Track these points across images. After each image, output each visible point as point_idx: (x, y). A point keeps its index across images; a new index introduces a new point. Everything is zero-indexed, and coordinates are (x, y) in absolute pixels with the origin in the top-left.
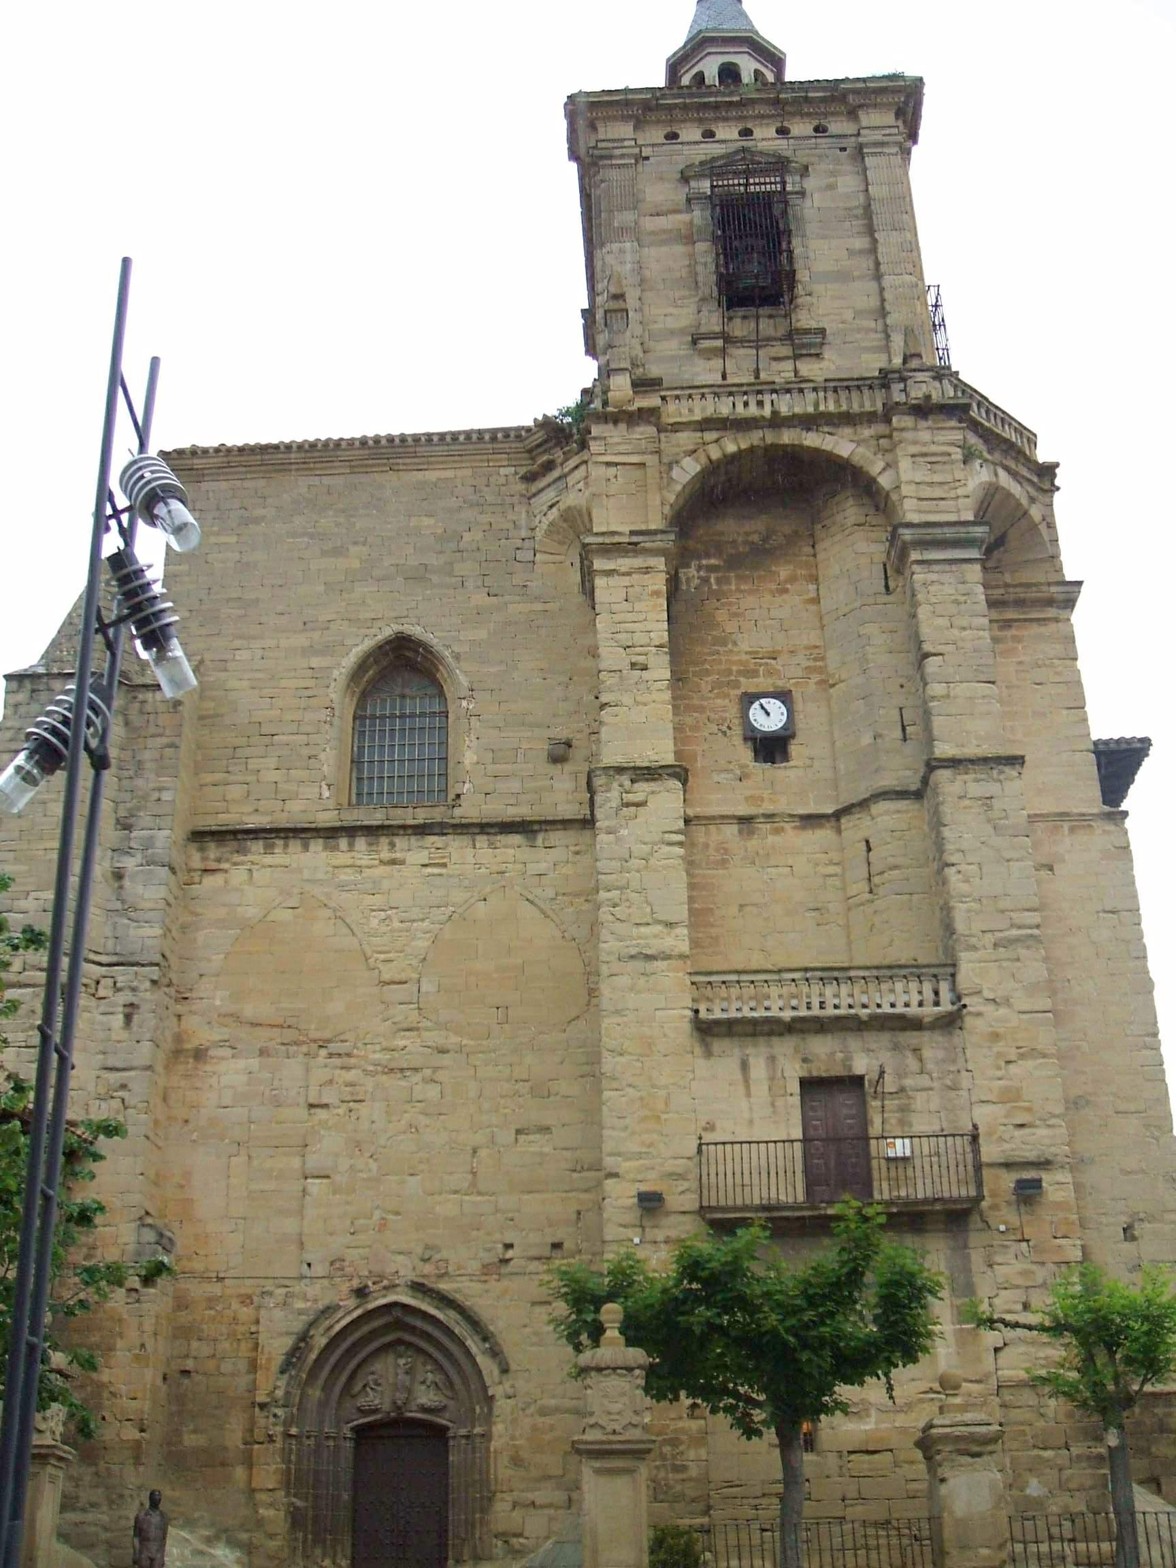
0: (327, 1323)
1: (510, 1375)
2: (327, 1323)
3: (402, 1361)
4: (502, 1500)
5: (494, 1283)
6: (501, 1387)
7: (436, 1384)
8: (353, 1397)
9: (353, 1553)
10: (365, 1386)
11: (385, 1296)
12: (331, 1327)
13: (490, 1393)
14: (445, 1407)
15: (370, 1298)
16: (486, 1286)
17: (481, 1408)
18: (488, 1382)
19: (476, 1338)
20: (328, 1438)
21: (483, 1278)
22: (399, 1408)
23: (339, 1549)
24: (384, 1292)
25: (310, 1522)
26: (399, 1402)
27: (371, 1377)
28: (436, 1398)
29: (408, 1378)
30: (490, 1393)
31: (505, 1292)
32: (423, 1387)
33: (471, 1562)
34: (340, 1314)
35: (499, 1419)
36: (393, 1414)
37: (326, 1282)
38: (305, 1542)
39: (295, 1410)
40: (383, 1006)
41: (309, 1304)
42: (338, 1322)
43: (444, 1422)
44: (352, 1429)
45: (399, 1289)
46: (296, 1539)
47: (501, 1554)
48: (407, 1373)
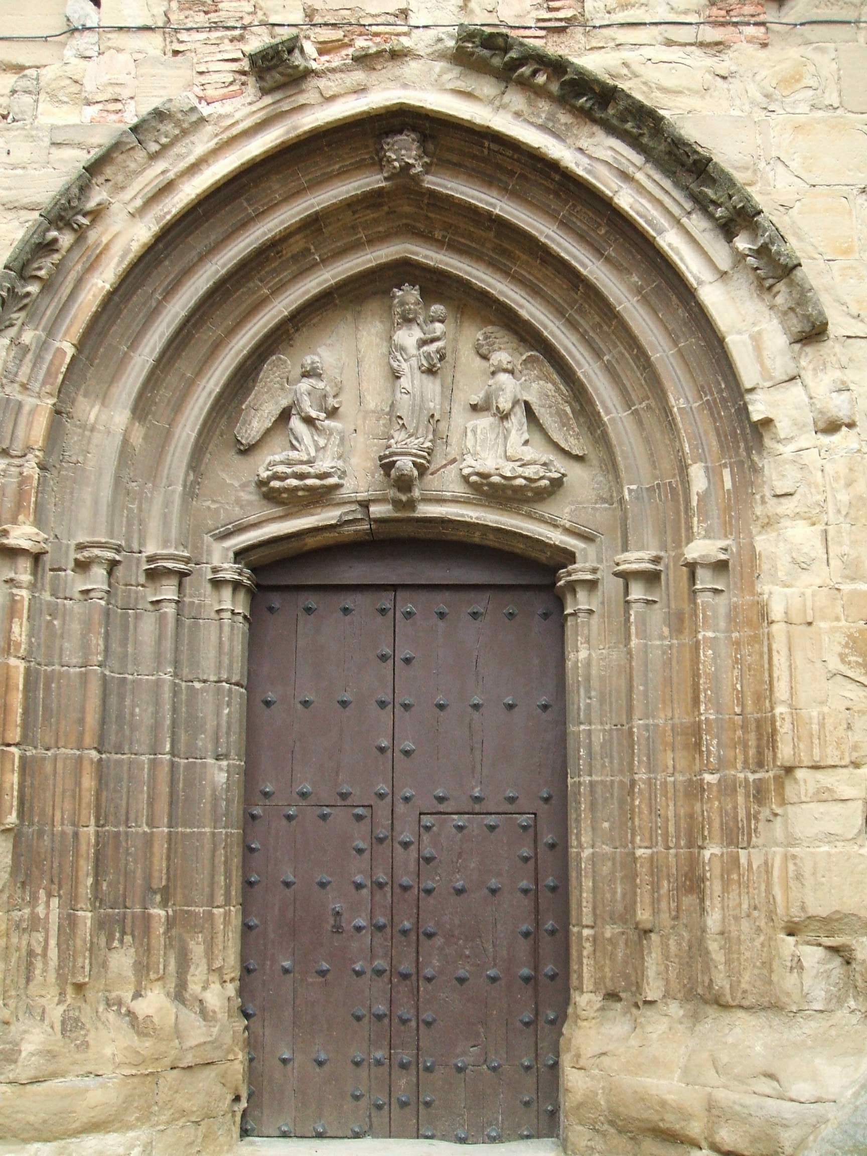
0: (154, 174)
1: (830, 348)
2: (154, 174)
3: (409, 337)
4: (825, 796)
5: (751, 50)
6: (796, 391)
7: (528, 407)
8: (247, 451)
9: (244, 957)
10: (285, 416)
11: (360, 90)
12: (168, 188)
13: (757, 412)
14: (557, 484)
15: (309, 96)
16: (725, 64)
17: (713, 474)
18: (748, 374)
19: (697, 224)
20: (154, 575)
21: (711, 34)
22: (404, 484)
23: (197, 949)
24: (358, 76)
25: (86, 866)
26: (405, 464)
27: (305, 385)
28: (529, 453)
29: (432, 388)
30: (757, 412)
31: (792, 80)
32: (485, 422)
33: (675, 1009)
34: (201, 144)
35: (788, 506)
36: (377, 510)
37: (153, 43)
38: (69, 923)
39: (31, 468)
40: (252, 9)
41: (92, 111)
42: (194, 168)
43: (557, 537)
44: (240, 555)
45: (412, 68)
46: (35, 924)
47: (819, 995)
48: (431, 371)
